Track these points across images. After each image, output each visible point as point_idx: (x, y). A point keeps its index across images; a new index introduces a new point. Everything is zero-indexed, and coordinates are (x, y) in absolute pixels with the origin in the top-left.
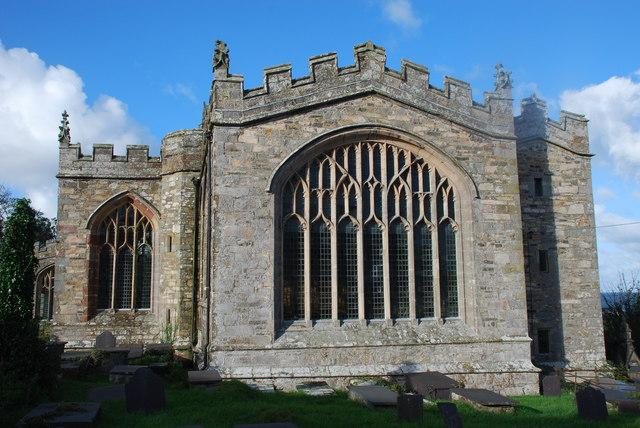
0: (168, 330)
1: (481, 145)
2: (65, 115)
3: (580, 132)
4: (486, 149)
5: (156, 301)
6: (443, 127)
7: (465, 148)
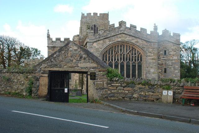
0: (76, 85)
2: (48, 30)
3: (178, 38)
4: (150, 45)
5: (73, 78)
6: (139, 40)
7: (144, 45)
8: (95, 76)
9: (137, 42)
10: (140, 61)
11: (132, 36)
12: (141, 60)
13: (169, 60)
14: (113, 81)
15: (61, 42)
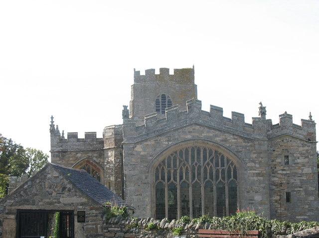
1: (249, 144)
2: (52, 118)
3: (310, 130)
4: (251, 146)
6: (230, 138)
7: (240, 146)
8: (84, 216)
9: (225, 140)
10: (232, 178)
11: (214, 129)
12: (235, 177)
13: (294, 176)
14: (110, 224)
15: (79, 140)
